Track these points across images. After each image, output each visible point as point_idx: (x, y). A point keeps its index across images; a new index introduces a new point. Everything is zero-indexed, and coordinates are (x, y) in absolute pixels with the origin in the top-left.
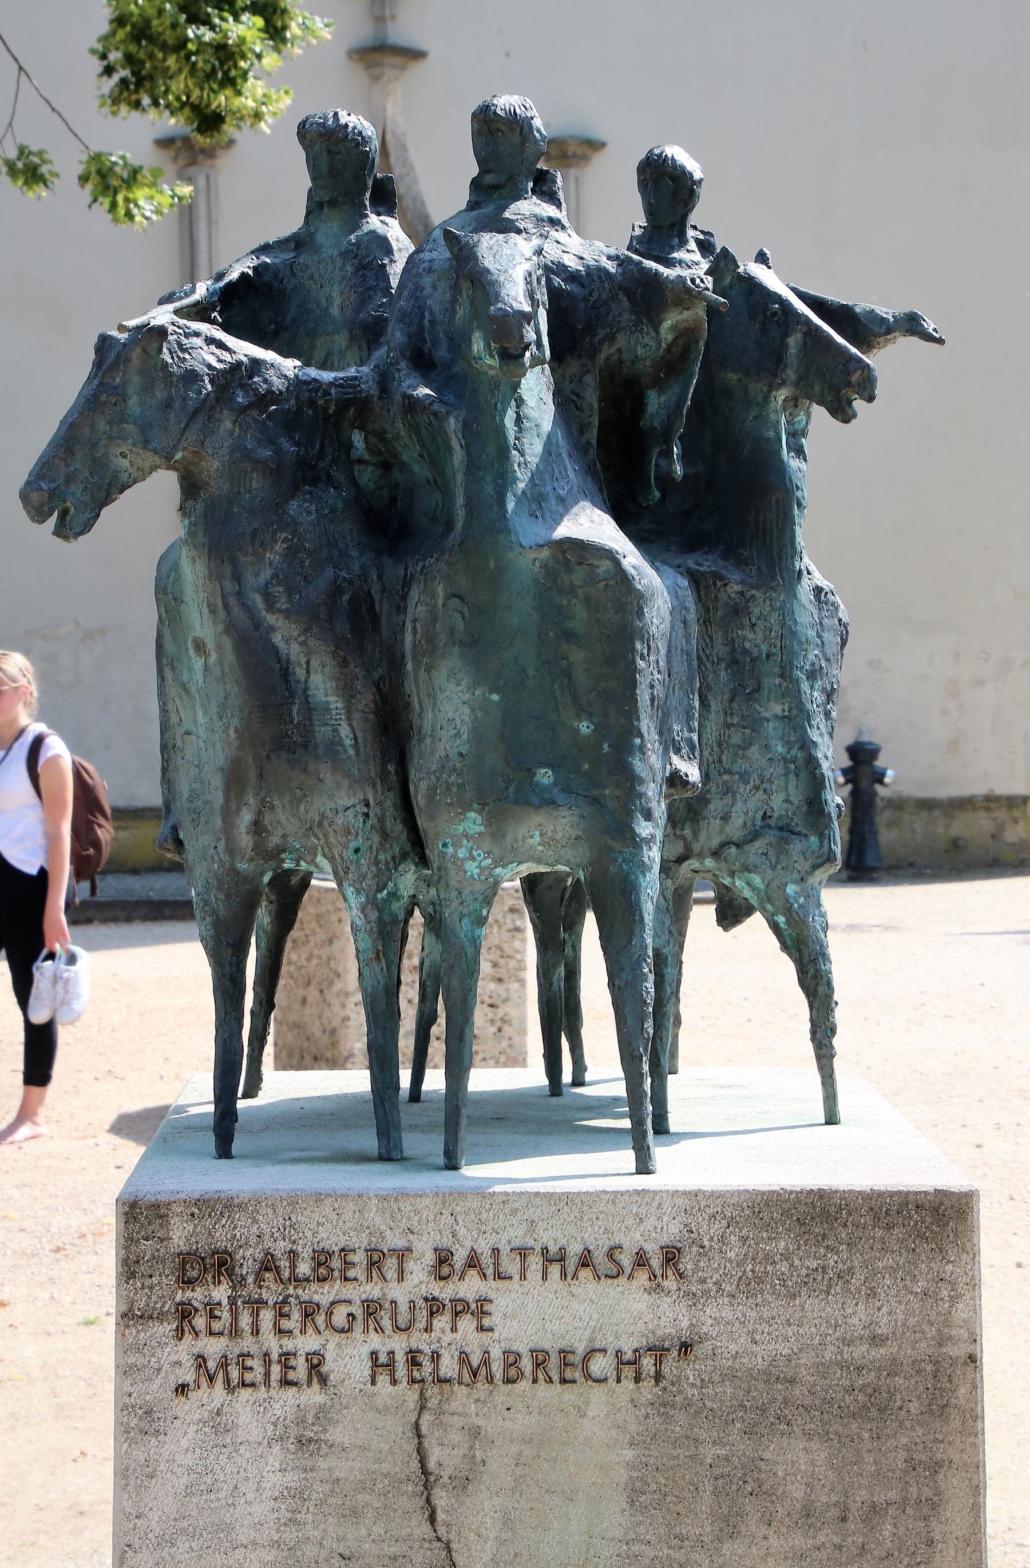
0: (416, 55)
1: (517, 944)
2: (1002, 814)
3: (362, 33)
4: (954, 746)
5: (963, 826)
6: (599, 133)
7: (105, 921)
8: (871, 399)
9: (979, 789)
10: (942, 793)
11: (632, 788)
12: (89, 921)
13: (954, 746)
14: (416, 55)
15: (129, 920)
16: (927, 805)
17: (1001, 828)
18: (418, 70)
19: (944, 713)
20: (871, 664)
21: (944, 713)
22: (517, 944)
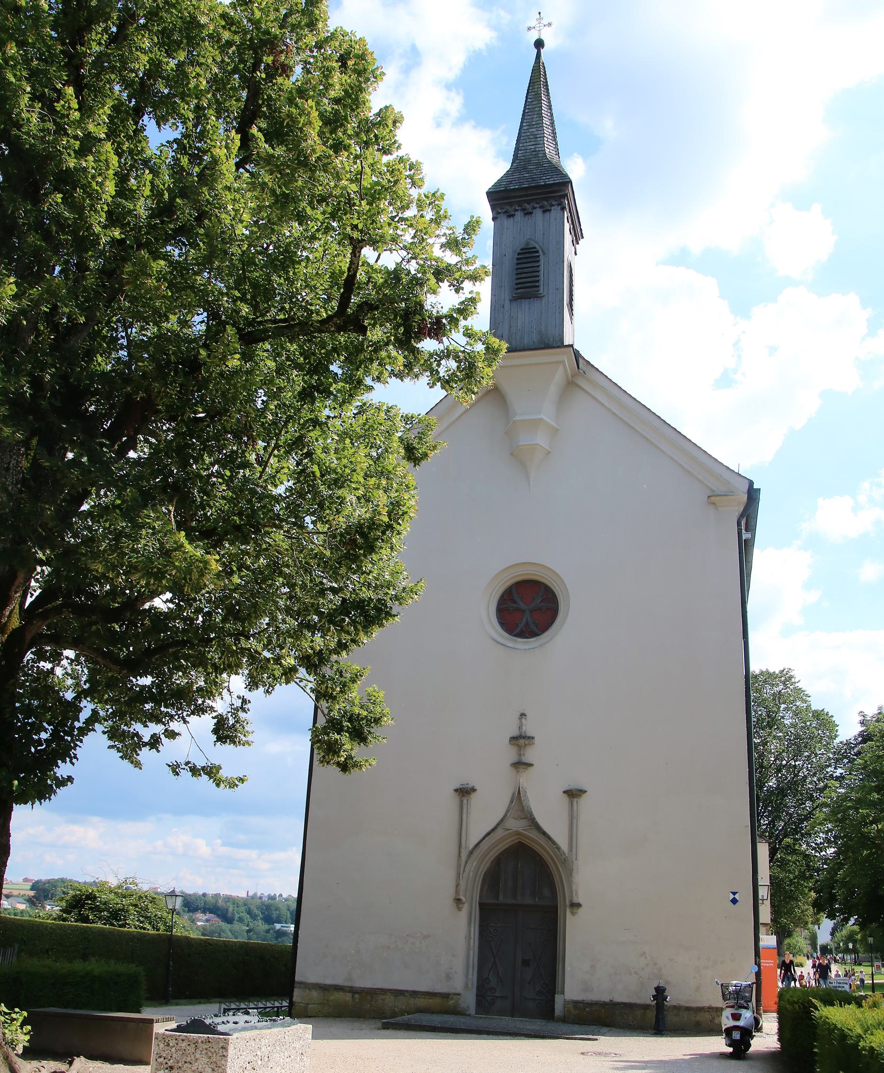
0: (531, 765)
1: (223, 1062)
2: (714, 1014)
3: (515, 759)
4: (698, 989)
5: (700, 1017)
6: (584, 788)
7: (393, 1029)
8: (219, 768)
9: (707, 1005)
10: (694, 1005)
11: (780, 1000)
12: (388, 1029)
13: (698, 989)
14: (531, 765)
15: (400, 1029)
16: (688, 1009)
17: (714, 1018)
18: (531, 769)
19: (695, 977)
20: (670, 960)
21: (695, 977)
22: (223, 1062)
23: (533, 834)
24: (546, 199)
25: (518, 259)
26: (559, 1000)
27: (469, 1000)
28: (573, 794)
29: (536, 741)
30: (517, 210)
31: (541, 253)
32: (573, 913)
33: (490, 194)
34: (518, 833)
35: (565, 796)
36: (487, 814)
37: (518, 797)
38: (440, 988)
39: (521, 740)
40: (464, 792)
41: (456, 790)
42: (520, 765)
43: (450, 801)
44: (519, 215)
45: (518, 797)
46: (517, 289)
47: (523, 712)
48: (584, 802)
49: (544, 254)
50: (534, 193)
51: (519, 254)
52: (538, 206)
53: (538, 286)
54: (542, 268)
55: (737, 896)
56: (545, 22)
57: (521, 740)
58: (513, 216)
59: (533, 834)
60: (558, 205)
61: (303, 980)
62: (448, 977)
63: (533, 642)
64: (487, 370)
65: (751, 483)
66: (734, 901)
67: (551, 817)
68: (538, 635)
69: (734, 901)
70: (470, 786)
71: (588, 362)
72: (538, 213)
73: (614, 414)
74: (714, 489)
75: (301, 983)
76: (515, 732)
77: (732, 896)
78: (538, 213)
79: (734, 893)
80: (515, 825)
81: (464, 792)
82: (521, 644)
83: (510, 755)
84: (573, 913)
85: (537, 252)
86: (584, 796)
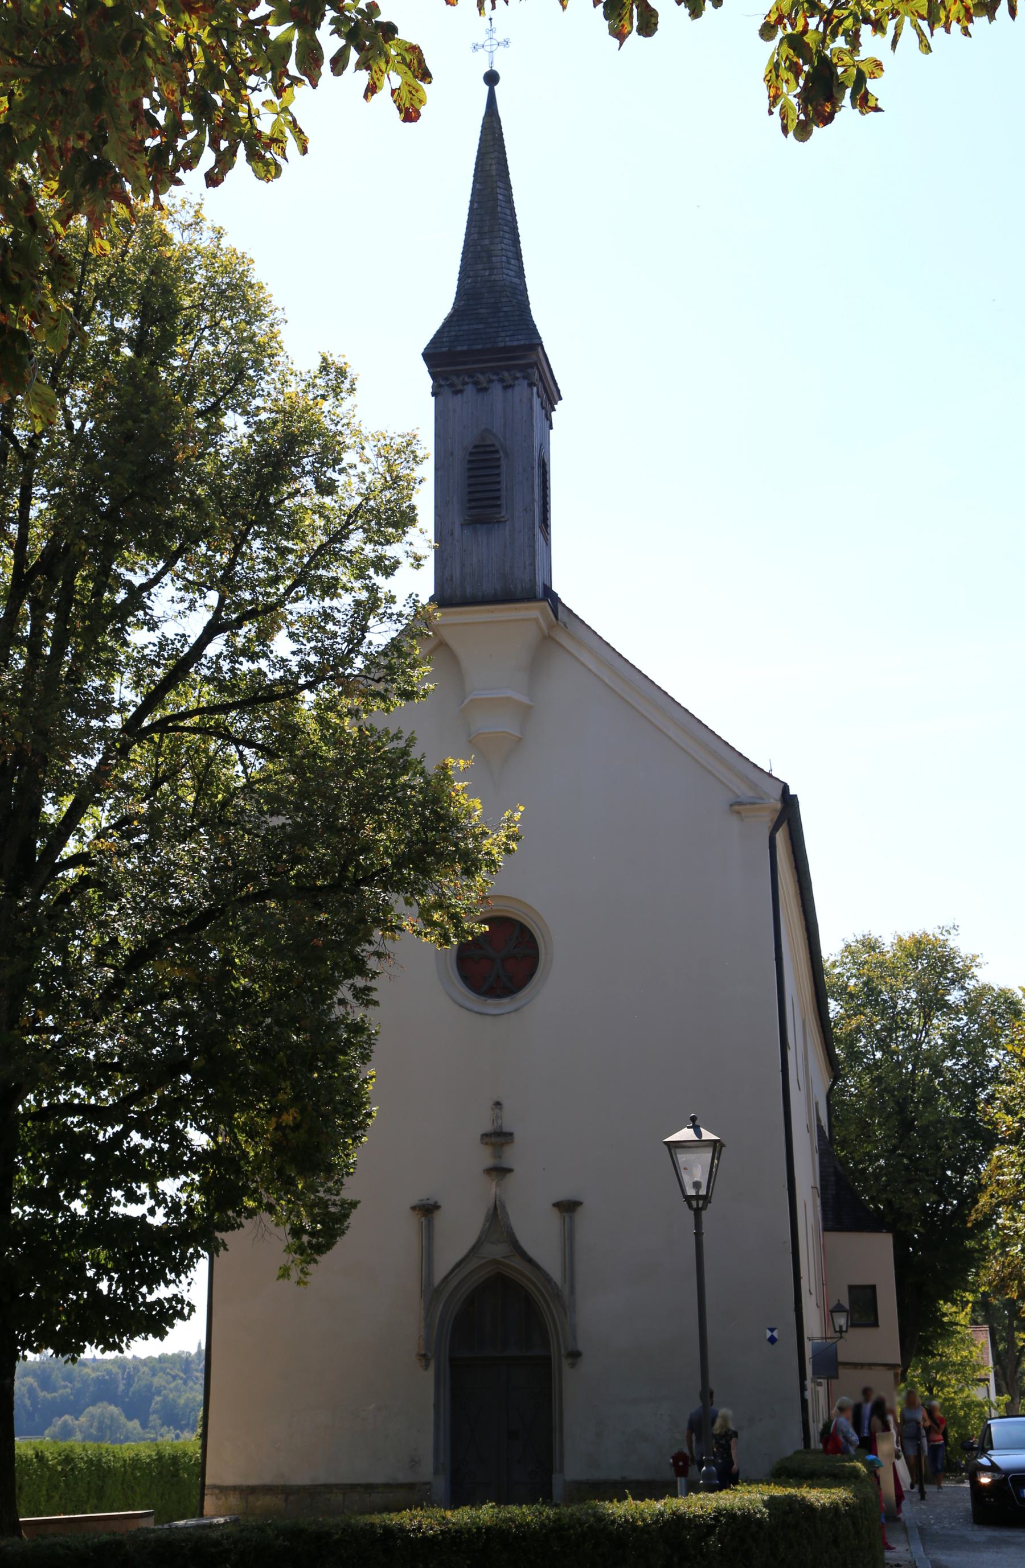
0: (510, 1170)
3: (489, 1162)
6: (581, 1200)
23: (517, 1263)
24: (508, 369)
25: (470, 462)
26: (557, 1479)
27: (441, 1486)
28: (568, 1207)
29: (517, 1137)
30: (467, 383)
31: (502, 454)
32: (573, 1365)
33: (429, 356)
34: (495, 1262)
35: (556, 1211)
36: (458, 1236)
37: (496, 1218)
38: (403, 1478)
39: (498, 1138)
40: (427, 1210)
41: (413, 1208)
42: (499, 1172)
43: (409, 1226)
44: (469, 389)
45: (496, 1218)
46: (470, 508)
47: (496, 1099)
48: (581, 1216)
49: (506, 454)
50: (490, 352)
51: (471, 454)
52: (495, 377)
53: (499, 506)
54: (503, 485)
55: (775, 1334)
56: (499, 37)
57: (498, 1138)
58: (461, 391)
59: (517, 1263)
60: (525, 378)
61: (218, 1482)
62: (414, 1463)
63: (506, 1004)
64: (144, 205)
65: (786, 787)
66: (772, 1340)
67: (538, 1236)
68: (515, 993)
69: (772, 1340)
70: (431, 1202)
71: (570, 611)
72: (497, 389)
73: (606, 684)
74: (739, 794)
75: (215, 1487)
76: (488, 1127)
77: (769, 1334)
78: (497, 389)
79: (772, 1330)
80: (496, 1251)
81: (427, 1210)
82: (492, 1006)
83: (485, 1157)
84: (573, 1365)
85: (497, 452)
86: (579, 1209)
